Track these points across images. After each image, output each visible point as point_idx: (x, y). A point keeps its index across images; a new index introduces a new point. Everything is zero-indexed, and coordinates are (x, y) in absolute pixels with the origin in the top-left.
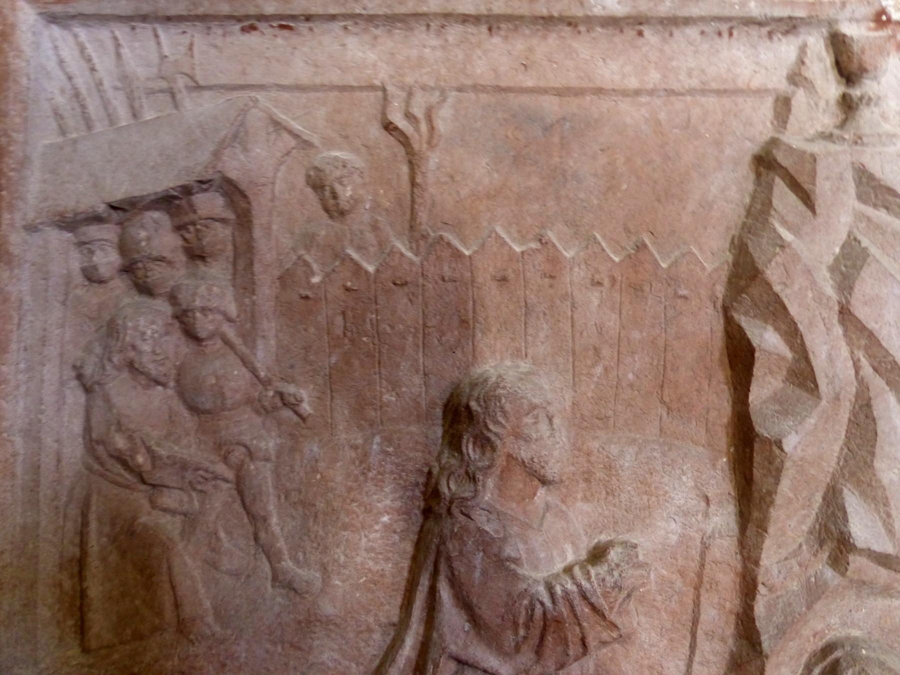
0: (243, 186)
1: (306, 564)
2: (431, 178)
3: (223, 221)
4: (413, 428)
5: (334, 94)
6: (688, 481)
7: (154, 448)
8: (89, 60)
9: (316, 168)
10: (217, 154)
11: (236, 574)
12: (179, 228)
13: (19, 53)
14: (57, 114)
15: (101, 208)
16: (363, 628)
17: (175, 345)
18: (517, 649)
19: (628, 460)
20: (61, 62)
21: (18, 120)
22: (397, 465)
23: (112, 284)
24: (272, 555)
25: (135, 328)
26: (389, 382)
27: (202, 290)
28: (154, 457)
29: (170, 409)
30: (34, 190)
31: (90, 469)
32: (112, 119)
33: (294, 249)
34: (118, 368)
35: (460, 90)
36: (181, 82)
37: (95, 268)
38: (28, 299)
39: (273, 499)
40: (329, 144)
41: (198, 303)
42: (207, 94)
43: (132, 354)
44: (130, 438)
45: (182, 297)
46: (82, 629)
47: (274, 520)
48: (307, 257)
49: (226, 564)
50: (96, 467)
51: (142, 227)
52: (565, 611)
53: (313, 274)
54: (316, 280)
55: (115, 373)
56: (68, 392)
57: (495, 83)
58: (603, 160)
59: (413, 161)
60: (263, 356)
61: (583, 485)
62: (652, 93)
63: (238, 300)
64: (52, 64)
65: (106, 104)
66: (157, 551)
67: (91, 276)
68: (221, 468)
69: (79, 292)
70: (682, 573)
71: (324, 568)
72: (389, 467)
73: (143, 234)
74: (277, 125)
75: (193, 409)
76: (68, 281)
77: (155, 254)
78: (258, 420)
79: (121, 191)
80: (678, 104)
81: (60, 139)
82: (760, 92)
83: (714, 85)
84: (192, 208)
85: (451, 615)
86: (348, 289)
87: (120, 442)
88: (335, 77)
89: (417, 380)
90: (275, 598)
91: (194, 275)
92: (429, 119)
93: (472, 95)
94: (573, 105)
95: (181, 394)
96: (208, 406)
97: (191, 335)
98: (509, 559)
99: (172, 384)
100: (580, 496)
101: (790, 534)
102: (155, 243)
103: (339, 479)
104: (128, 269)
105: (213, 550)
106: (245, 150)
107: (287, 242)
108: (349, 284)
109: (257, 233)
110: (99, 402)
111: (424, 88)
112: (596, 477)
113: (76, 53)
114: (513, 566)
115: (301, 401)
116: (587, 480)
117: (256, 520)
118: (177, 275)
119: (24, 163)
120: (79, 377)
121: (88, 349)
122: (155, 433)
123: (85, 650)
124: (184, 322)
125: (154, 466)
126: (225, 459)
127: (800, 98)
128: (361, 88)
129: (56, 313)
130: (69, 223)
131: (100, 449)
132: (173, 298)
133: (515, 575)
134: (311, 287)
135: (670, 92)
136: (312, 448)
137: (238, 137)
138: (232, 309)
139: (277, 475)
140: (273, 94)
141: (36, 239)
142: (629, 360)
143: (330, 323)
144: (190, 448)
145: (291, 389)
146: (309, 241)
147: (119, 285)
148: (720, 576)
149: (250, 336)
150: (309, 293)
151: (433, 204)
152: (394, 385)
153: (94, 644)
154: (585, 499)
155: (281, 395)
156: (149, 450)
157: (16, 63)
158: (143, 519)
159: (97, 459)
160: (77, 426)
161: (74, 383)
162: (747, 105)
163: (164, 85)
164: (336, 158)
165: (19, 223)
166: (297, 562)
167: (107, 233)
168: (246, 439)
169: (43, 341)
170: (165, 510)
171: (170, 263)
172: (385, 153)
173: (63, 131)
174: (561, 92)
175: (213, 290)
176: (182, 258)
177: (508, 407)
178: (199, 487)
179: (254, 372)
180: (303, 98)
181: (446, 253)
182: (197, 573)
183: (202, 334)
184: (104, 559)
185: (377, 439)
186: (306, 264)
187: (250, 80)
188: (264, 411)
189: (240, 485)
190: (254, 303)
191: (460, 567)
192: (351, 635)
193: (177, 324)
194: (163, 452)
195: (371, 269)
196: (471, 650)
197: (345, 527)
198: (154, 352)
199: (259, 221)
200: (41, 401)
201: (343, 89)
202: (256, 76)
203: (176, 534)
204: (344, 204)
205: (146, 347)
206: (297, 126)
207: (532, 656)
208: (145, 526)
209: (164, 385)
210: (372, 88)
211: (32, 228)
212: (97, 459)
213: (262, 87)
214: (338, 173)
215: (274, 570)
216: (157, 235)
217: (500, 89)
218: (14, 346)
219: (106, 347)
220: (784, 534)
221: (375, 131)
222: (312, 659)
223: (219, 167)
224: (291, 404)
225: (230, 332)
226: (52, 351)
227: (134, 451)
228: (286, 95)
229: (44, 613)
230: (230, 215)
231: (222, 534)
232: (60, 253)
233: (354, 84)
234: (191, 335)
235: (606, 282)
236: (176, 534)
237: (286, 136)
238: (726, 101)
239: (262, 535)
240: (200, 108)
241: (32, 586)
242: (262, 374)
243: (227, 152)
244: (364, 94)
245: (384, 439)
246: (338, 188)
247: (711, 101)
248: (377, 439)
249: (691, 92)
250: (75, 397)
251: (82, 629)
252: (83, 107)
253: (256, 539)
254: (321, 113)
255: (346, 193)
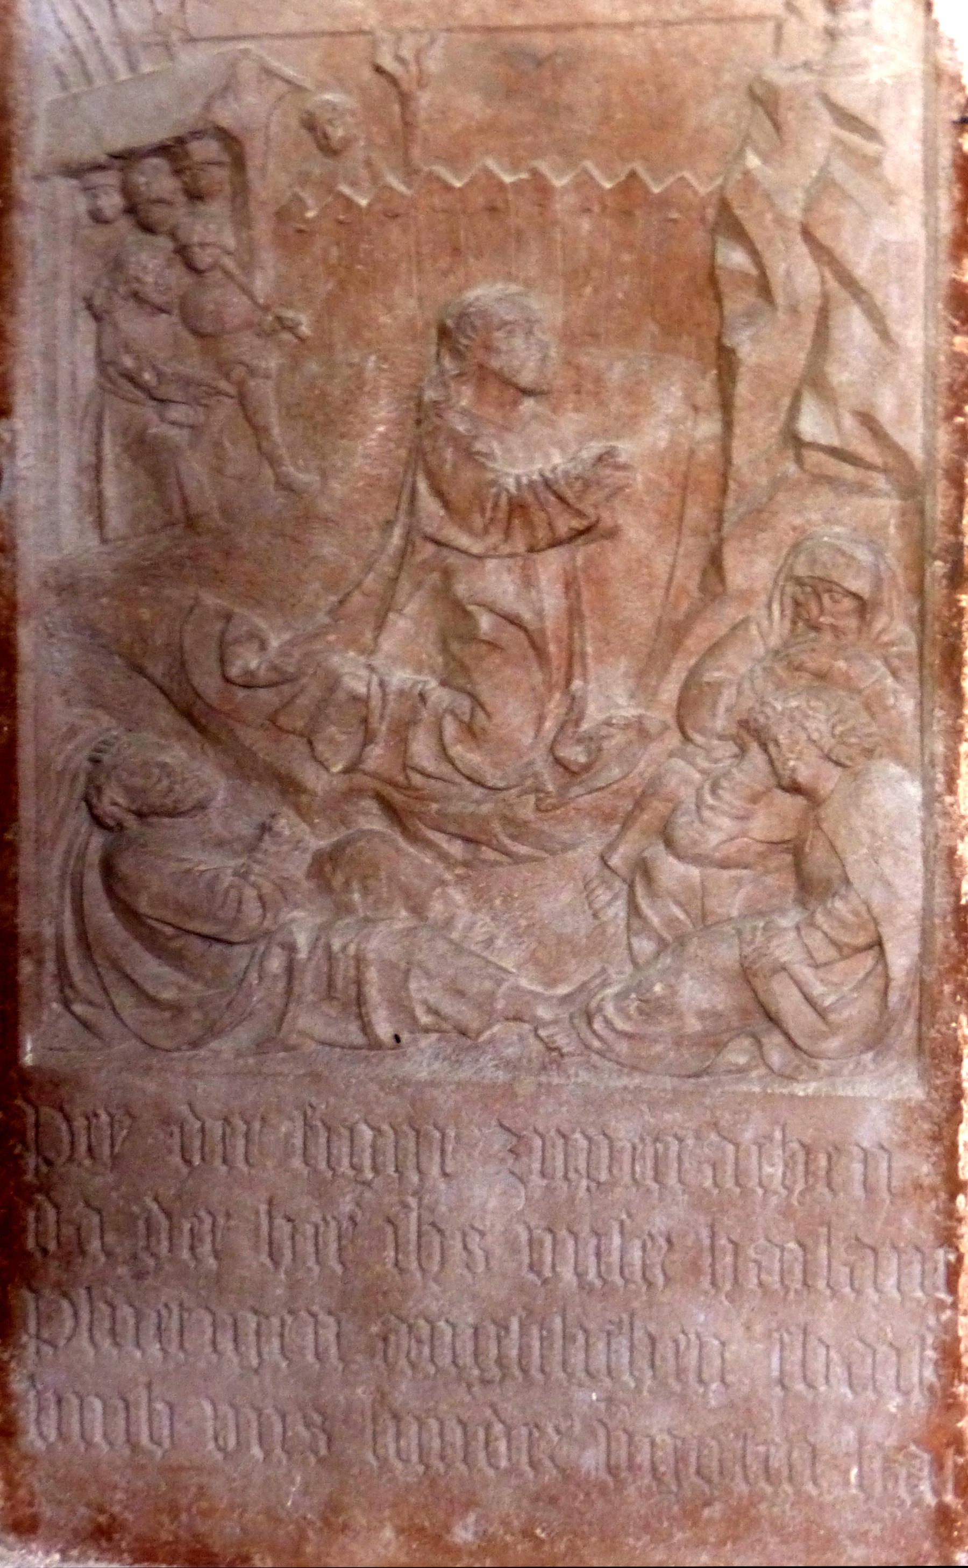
0: (236, 132)
1: (306, 470)
2: (422, 115)
3: (219, 164)
4: (409, 348)
5: (325, 40)
6: (677, 391)
7: (160, 366)
8: (86, 20)
9: (308, 112)
10: (207, 107)
11: (241, 479)
12: (177, 172)
13: (21, 22)
14: (60, 73)
15: (103, 159)
16: (362, 526)
17: (177, 277)
18: (486, 531)
19: (617, 373)
20: (60, 24)
21: (23, 84)
22: (393, 380)
23: (117, 224)
24: (274, 462)
25: (138, 263)
26: (385, 305)
27: (199, 228)
28: (160, 375)
29: (175, 334)
30: (38, 143)
31: (102, 387)
32: (111, 73)
33: (290, 186)
34: (125, 298)
35: (449, 30)
36: (175, 36)
37: (99, 210)
38: (40, 240)
39: (274, 412)
40: (323, 86)
41: (196, 239)
42: (201, 45)
43: (136, 286)
44: (137, 358)
45: (180, 233)
46: (100, 523)
47: (276, 431)
48: (303, 195)
49: (230, 469)
50: (109, 386)
51: (142, 174)
52: (530, 498)
53: (307, 209)
54: (310, 214)
55: (121, 302)
56: (80, 321)
57: (481, 23)
58: (597, 90)
59: (405, 99)
60: (261, 284)
61: (572, 397)
62: (646, 23)
63: (237, 235)
64: (51, 26)
65: (104, 60)
66: (165, 456)
67: (97, 217)
68: (223, 385)
69: (87, 232)
70: (670, 475)
71: (324, 475)
72: (384, 382)
73: (142, 180)
74: (269, 73)
75: (197, 333)
76: (76, 222)
77: (154, 196)
78: (258, 342)
79: (120, 140)
80: (675, 33)
81: (62, 95)
82: (759, 18)
83: (710, 15)
84: (187, 155)
85: (429, 504)
86: (341, 223)
87: (128, 362)
88: (324, 24)
89: (412, 303)
90: (280, 500)
91: (191, 214)
92: (418, 60)
93: (462, 36)
94: (564, 40)
95: (186, 319)
96: (210, 329)
97: (191, 267)
98: (478, 453)
99: (176, 311)
100: (570, 406)
101: (759, 434)
102: (155, 187)
103: (337, 393)
104: (131, 210)
105: (219, 458)
106: (237, 99)
107: (283, 178)
108: (341, 217)
109: (252, 174)
110: (109, 329)
111: (413, 31)
112: (586, 388)
113: (74, 14)
114: (483, 460)
115: (299, 324)
116: (578, 392)
117: (259, 431)
118: (180, 214)
119: (32, 119)
120: (90, 307)
121: (97, 283)
122: (161, 355)
123: (104, 541)
124: (183, 253)
125: (160, 382)
126: (227, 376)
127: (792, 26)
128: (351, 33)
129: (67, 251)
130: (74, 171)
131: (111, 370)
132: (173, 235)
133: (483, 466)
134: (306, 221)
135: (667, 24)
136: (313, 367)
137: (229, 87)
138: (230, 241)
139: (278, 391)
140: (266, 42)
141: (44, 187)
142: (618, 281)
143: (326, 251)
144: (194, 366)
145: (289, 314)
146: (304, 179)
147: (124, 224)
148: (704, 477)
149: (248, 267)
150: (303, 227)
151: (426, 139)
152: (390, 309)
153: (111, 535)
154: (577, 410)
155: (279, 319)
156: (154, 367)
157: (18, 32)
158: (153, 430)
159: (110, 379)
160: (89, 351)
161: (85, 313)
162: (747, 31)
163: (159, 38)
164: (328, 102)
165: (28, 173)
166: (298, 468)
167: (110, 179)
168: (246, 358)
169: (55, 276)
170: (173, 423)
171: (169, 203)
172: (377, 93)
173: (64, 87)
174: (553, 28)
175: (212, 229)
176: (181, 198)
177: (478, 323)
178: (204, 402)
179: (252, 297)
180: (294, 45)
181: (436, 186)
182: (205, 479)
183: (201, 266)
184: (117, 466)
185: (373, 358)
186: (300, 200)
187: (242, 31)
188: (267, 334)
189: (242, 399)
190: (251, 238)
191: (432, 460)
192: (352, 533)
193: (178, 258)
194: (168, 370)
195: (364, 202)
196: (445, 532)
197: (342, 436)
198: (156, 283)
199: (253, 163)
200: (55, 329)
201: (335, 34)
202: (248, 26)
203: (184, 445)
204: (335, 143)
205: (149, 279)
206: (290, 72)
207: (501, 536)
208: (155, 436)
209: (167, 312)
210: (361, 32)
211: (39, 178)
212: (110, 379)
213: (253, 37)
214: (328, 116)
215: (277, 475)
216: (157, 180)
217: (488, 30)
218: (29, 282)
219: (114, 282)
220: (751, 434)
221: (367, 74)
222: (312, 552)
223: (210, 117)
224: (292, 328)
225: (229, 263)
226: (64, 285)
227: (141, 370)
228: (278, 43)
229: (66, 509)
230: (225, 158)
231: (227, 444)
232: (69, 199)
233: (343, 29)
234: (191, 267)
235: (596, 209)
236: (184, 445)
237: (279, 83)
238: (726, 29)
239: (264, 444)
240: (194, 61)
241: (54, 485)
242: (261, 301)
243: (219, 103)
244: (354, 39)
245: (379, 358)
246: (329, 129)
247: (708, 29)
248: (373, 358)
249: (689, 21)
250: (86, 325)
251: (100, 523)
252: (83, 63)
253: (259, 447)
254: (314, 57)
255: (337, 133)
